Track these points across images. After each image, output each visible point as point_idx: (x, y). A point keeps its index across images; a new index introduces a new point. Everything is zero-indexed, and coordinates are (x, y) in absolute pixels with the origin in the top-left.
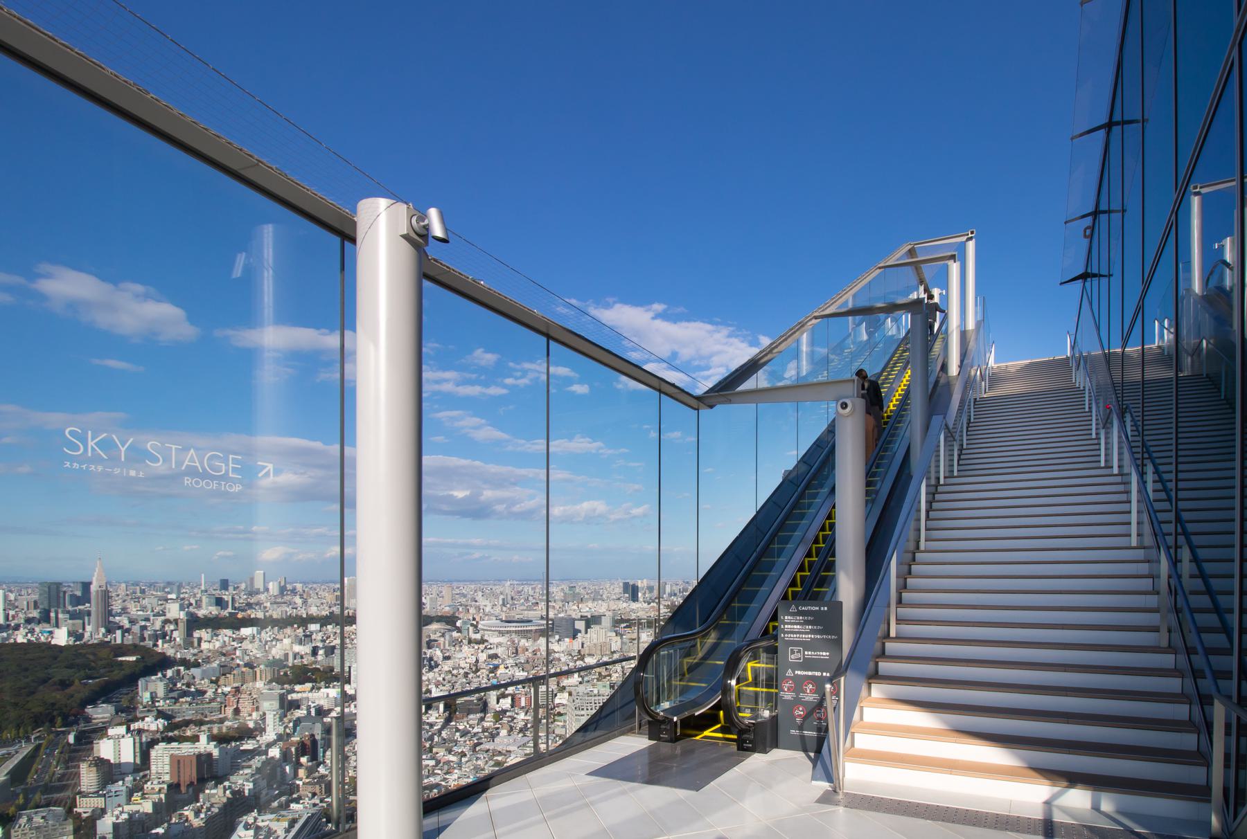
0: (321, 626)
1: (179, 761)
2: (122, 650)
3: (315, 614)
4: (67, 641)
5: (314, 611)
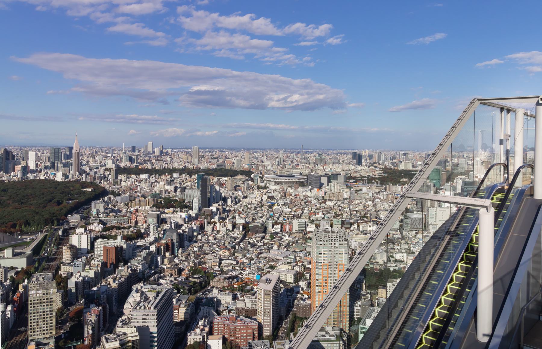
0: (179, 175)
2: (85, 185)
5: (176, 165)
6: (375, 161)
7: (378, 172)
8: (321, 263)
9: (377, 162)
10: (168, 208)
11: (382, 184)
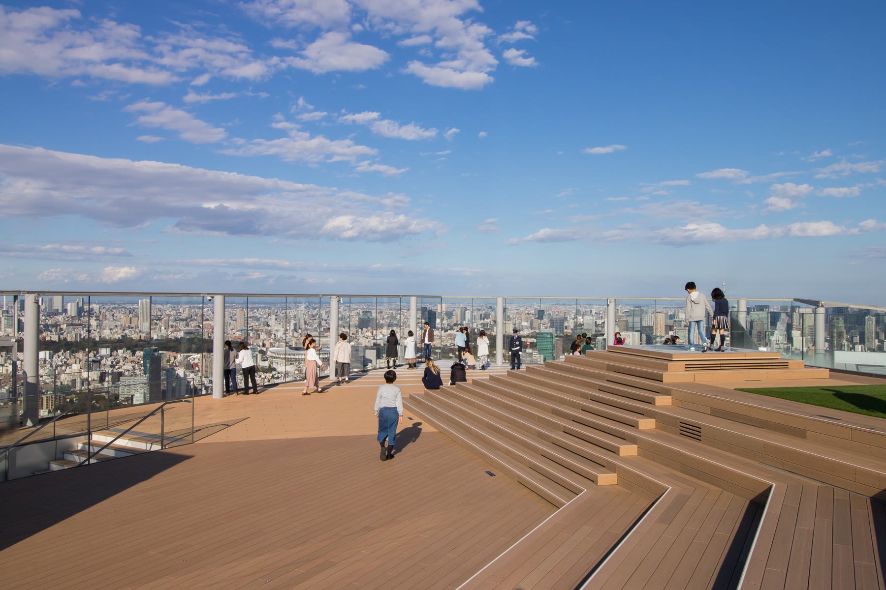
0: (112, 351)
3: (107, 338)
5: (107, 334)
6: (457, 321)
9: (459, 322)
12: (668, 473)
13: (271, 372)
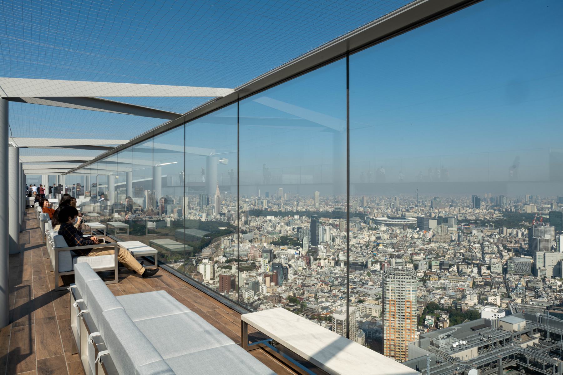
0: (300, 217)
1: (222, 277)
2: (222, 224)
3: (299, 210)
4: (206, 220)
5: (299, 208)
7: (497, 215)
8: (389, 298)
10: (284, 245)
11: (496, 227)
12: (89, 167)
13: (376, 230)
